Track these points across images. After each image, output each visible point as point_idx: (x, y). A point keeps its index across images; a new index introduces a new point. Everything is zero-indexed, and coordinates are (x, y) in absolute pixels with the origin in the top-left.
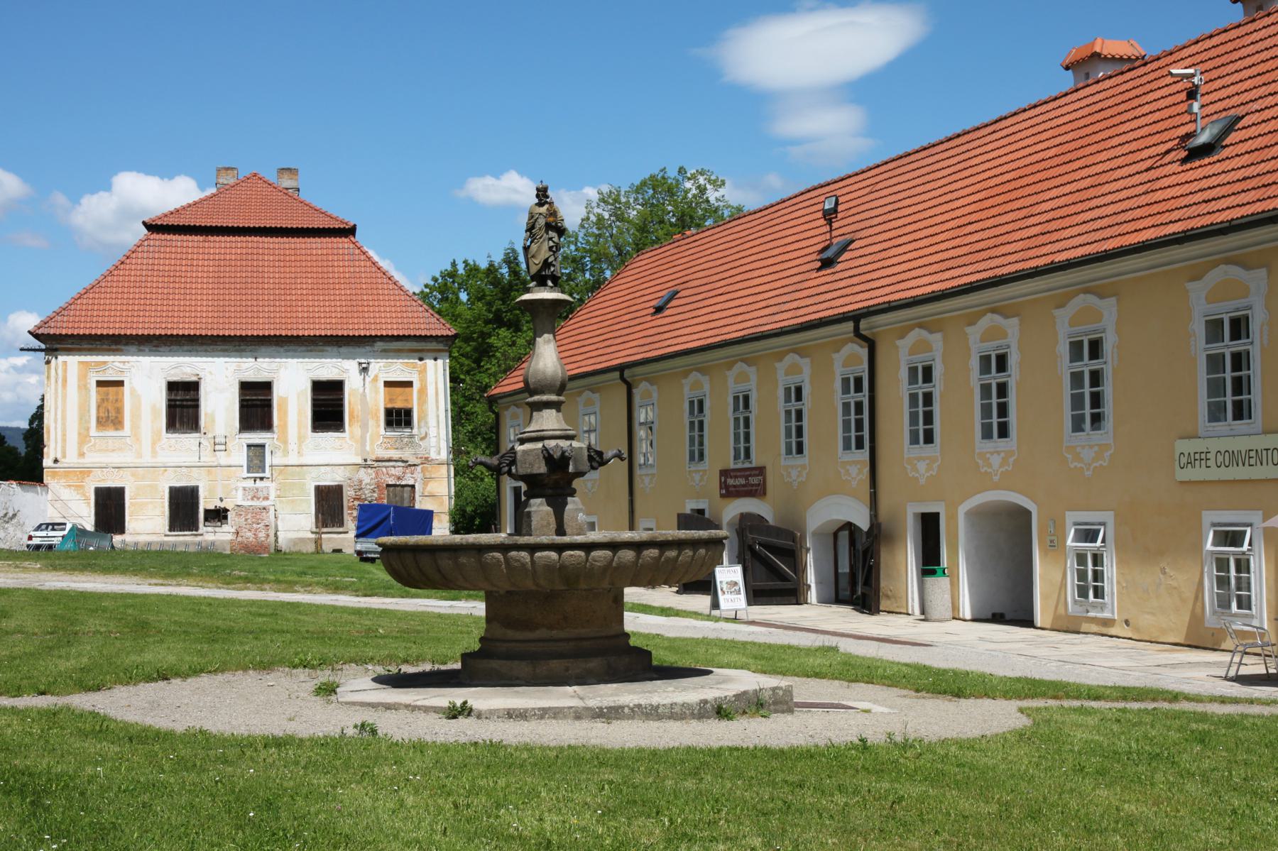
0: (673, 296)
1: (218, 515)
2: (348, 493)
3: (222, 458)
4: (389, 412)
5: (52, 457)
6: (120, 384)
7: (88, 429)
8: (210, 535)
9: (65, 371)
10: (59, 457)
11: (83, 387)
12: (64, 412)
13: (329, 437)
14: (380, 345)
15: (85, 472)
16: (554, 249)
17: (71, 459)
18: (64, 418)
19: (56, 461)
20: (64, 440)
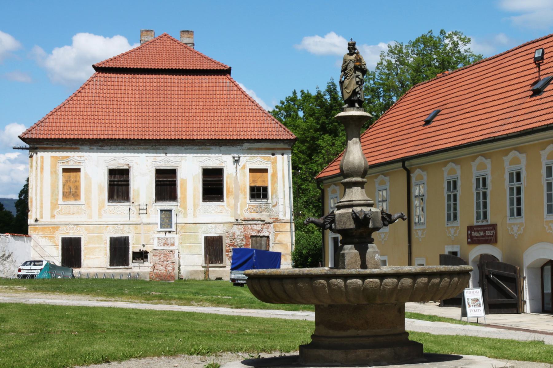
0: (437, 114)
1: (141, 256)
2: (226, 241)
3: (144, 219)
4: (252, 189)
6: (78, 170)
10: (38, 218)
11: (54, 172)
12: (41, 188)
13: (213, 205)
14: (246, 145)
15: (55, 227)
16: (360, 83)
17: (46, 219)
18: (41, 192)
19: (36, 220)
20: (42, 207)
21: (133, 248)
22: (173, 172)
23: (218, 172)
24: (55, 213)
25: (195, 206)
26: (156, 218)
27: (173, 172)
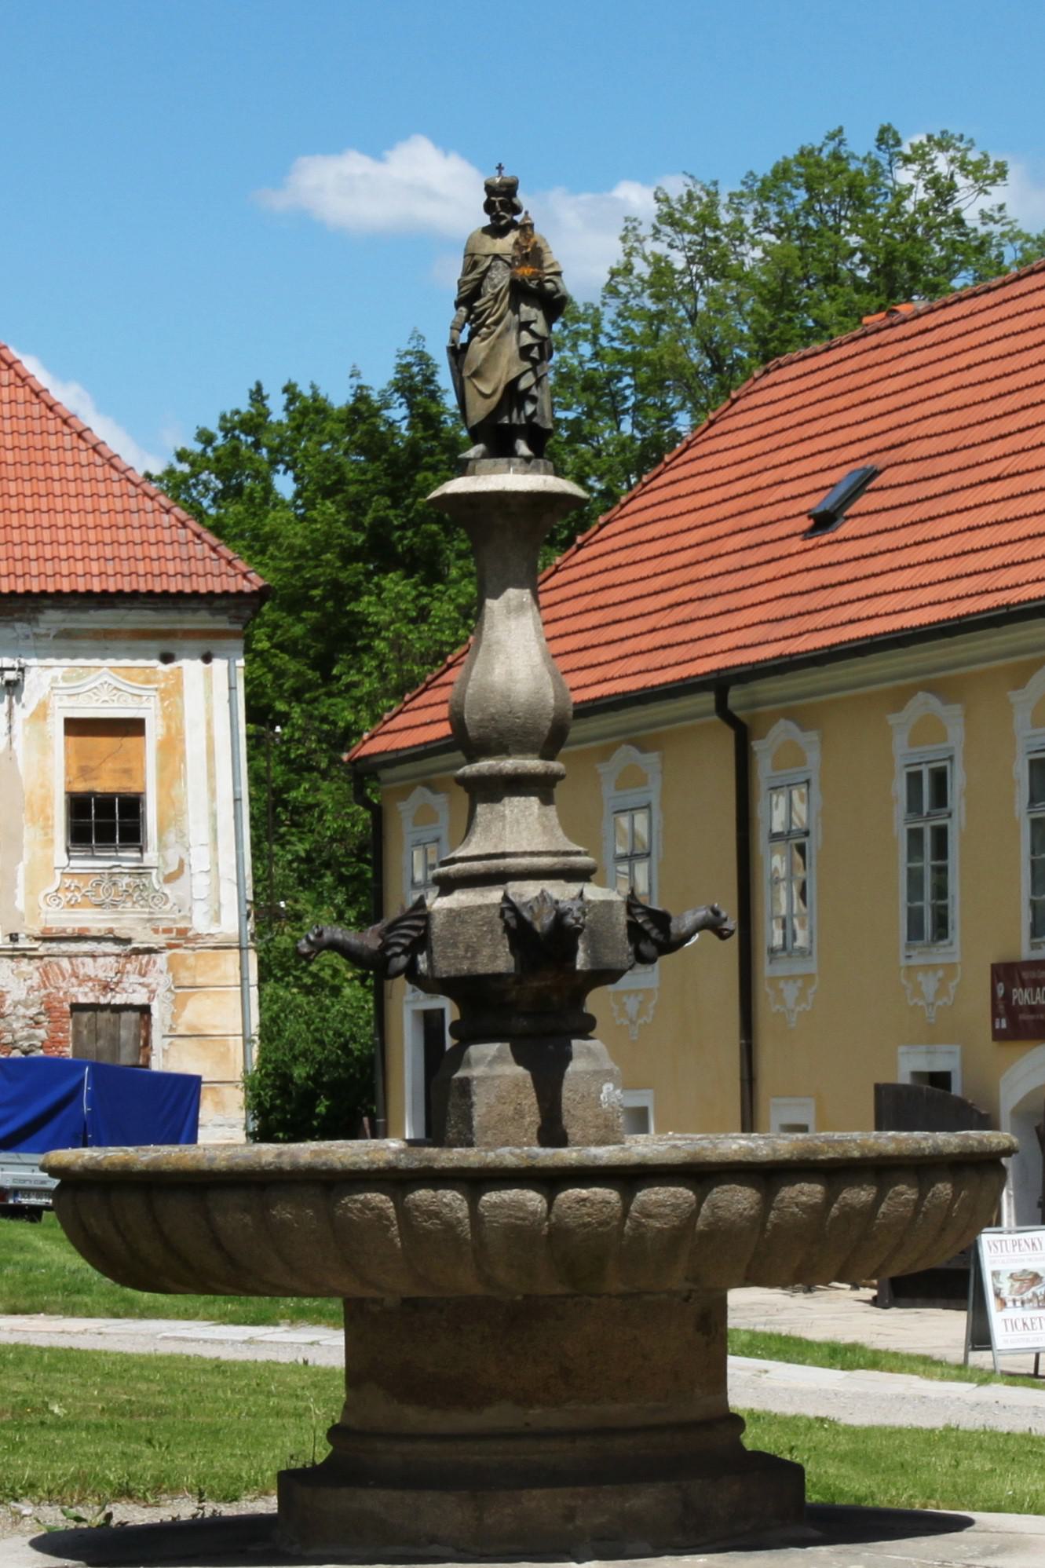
4: (78, 805)
14: (53, 619)
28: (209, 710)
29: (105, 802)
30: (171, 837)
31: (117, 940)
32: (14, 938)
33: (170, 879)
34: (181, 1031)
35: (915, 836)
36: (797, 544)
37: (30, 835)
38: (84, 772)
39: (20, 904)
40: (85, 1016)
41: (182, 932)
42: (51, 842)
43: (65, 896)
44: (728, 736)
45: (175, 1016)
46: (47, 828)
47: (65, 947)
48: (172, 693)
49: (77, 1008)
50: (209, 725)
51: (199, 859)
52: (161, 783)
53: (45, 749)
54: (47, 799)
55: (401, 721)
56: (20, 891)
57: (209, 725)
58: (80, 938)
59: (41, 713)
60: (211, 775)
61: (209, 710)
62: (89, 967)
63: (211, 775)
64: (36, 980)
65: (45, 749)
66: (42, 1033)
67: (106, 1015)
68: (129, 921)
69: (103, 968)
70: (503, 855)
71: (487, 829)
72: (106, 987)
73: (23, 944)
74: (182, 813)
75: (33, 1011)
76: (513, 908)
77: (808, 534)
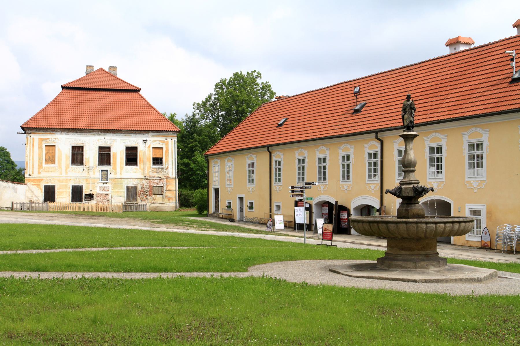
1: (90, 197)
2: (139, 188)
3: (92, 175)
4: (154, 159)
5: (28, 174)
7: (42, 163)
8: (86, 204)
9: (34, 141)
10: (31, 174)
11: (40, 147)
13: (132, 168)
14: (151, 133)
15: (40, 180)
17: (35, 175)
18: (33, 159)
19: (30, 175)
20: (33, 167)
21: (85, 192)
22: (109, 148)
23: (135, 149)
24: (41, 171)
25: (121, 168)
26: (98, 175)
27: (109, 148)
28: (172, 147)
29: (158, 159)
30: (166, 164)
31: (159, 177)
32: (145, 177)
33: (166, 169)
34: (168, 190)
35: (299, 168)
36: (275, 128)
37: (147, 163)
38: (155, 155)
39: (146, 172)
40: (155, 188)
41: (168, 176)
42: (150, 164)
43: (152, 171)
44: (269, 153)
45: (167, 188)
46: (150, 162)
47: (152, 178)
48: (167, 144)
49: (153, 186)
50: (172, 148)
51: (170, 167)
52: (165, 156)
53: (150, 151)
54: (150, 158)
55: (212, 150)
56: (146, 171)
57: (172, 148)
58: (154, 177)
59: (149, 146)
60: (172, 155)
61: (172, 147)
62: (155, 181)
63: (172, 155)
64: (148, 183)
65: (150, 151)
66: (149, 190)
67: (157, 187)
68: (161, 175)
69: (157, 181)
70: (411, 181)
71: (408, 177)
72: (157, 184)
73: (146, 178)
74: (168, 160)
75: (148, 187)
76: (415, 188)
77: (277, 127)
